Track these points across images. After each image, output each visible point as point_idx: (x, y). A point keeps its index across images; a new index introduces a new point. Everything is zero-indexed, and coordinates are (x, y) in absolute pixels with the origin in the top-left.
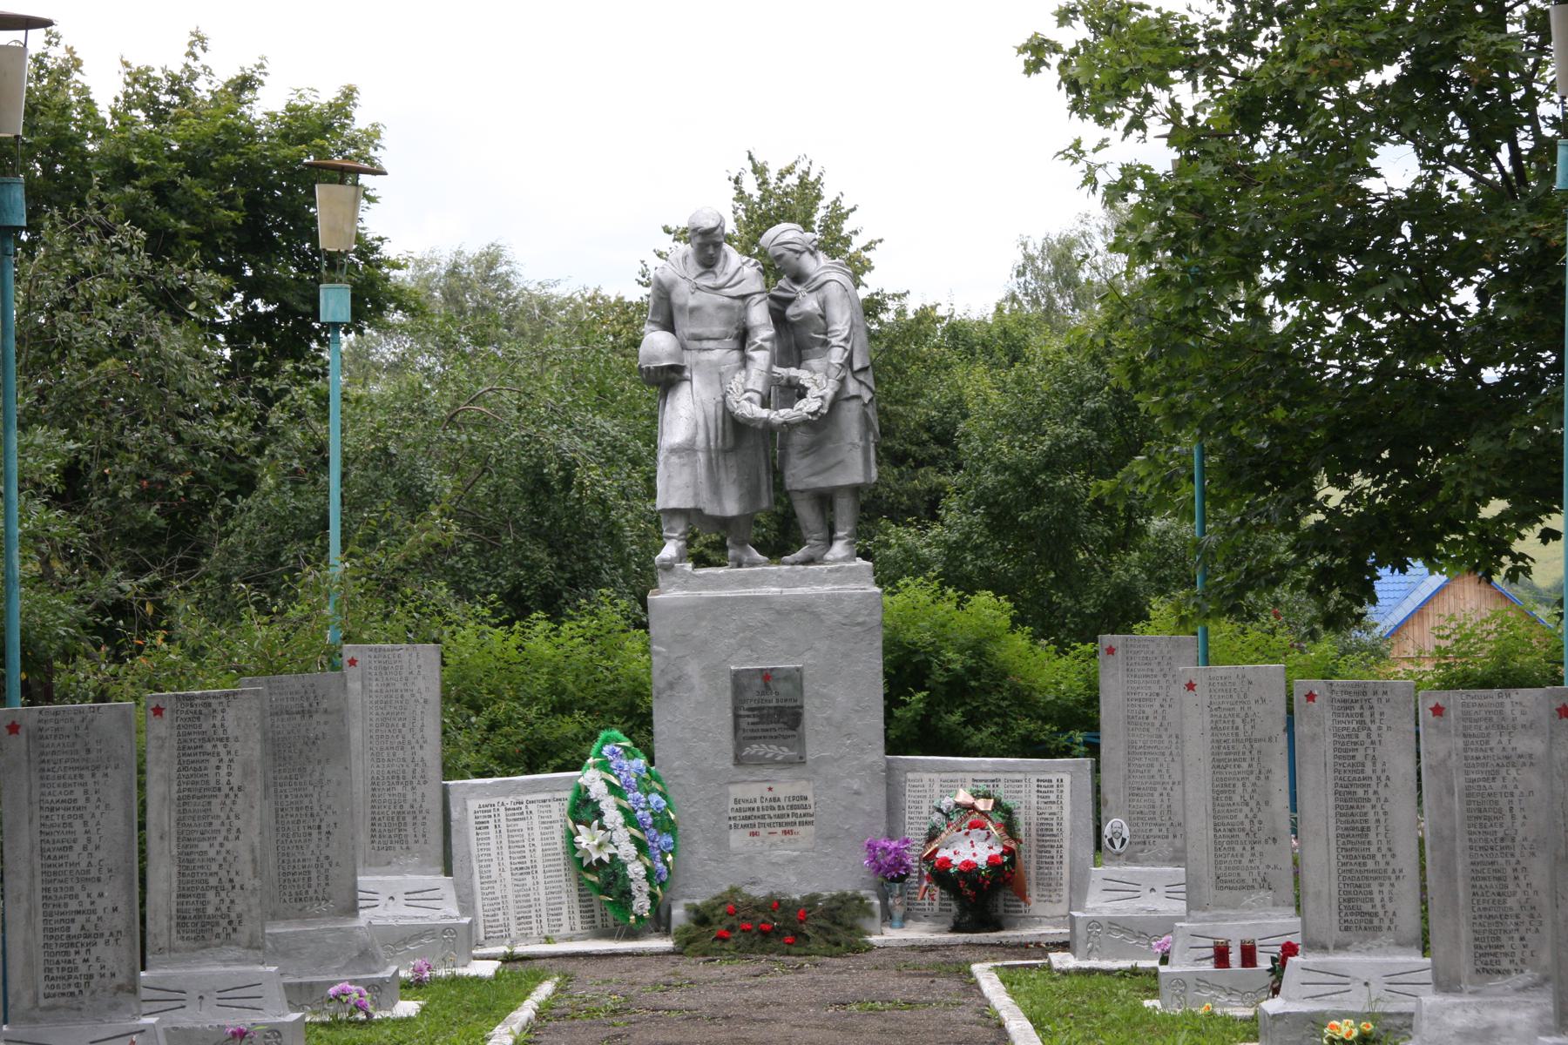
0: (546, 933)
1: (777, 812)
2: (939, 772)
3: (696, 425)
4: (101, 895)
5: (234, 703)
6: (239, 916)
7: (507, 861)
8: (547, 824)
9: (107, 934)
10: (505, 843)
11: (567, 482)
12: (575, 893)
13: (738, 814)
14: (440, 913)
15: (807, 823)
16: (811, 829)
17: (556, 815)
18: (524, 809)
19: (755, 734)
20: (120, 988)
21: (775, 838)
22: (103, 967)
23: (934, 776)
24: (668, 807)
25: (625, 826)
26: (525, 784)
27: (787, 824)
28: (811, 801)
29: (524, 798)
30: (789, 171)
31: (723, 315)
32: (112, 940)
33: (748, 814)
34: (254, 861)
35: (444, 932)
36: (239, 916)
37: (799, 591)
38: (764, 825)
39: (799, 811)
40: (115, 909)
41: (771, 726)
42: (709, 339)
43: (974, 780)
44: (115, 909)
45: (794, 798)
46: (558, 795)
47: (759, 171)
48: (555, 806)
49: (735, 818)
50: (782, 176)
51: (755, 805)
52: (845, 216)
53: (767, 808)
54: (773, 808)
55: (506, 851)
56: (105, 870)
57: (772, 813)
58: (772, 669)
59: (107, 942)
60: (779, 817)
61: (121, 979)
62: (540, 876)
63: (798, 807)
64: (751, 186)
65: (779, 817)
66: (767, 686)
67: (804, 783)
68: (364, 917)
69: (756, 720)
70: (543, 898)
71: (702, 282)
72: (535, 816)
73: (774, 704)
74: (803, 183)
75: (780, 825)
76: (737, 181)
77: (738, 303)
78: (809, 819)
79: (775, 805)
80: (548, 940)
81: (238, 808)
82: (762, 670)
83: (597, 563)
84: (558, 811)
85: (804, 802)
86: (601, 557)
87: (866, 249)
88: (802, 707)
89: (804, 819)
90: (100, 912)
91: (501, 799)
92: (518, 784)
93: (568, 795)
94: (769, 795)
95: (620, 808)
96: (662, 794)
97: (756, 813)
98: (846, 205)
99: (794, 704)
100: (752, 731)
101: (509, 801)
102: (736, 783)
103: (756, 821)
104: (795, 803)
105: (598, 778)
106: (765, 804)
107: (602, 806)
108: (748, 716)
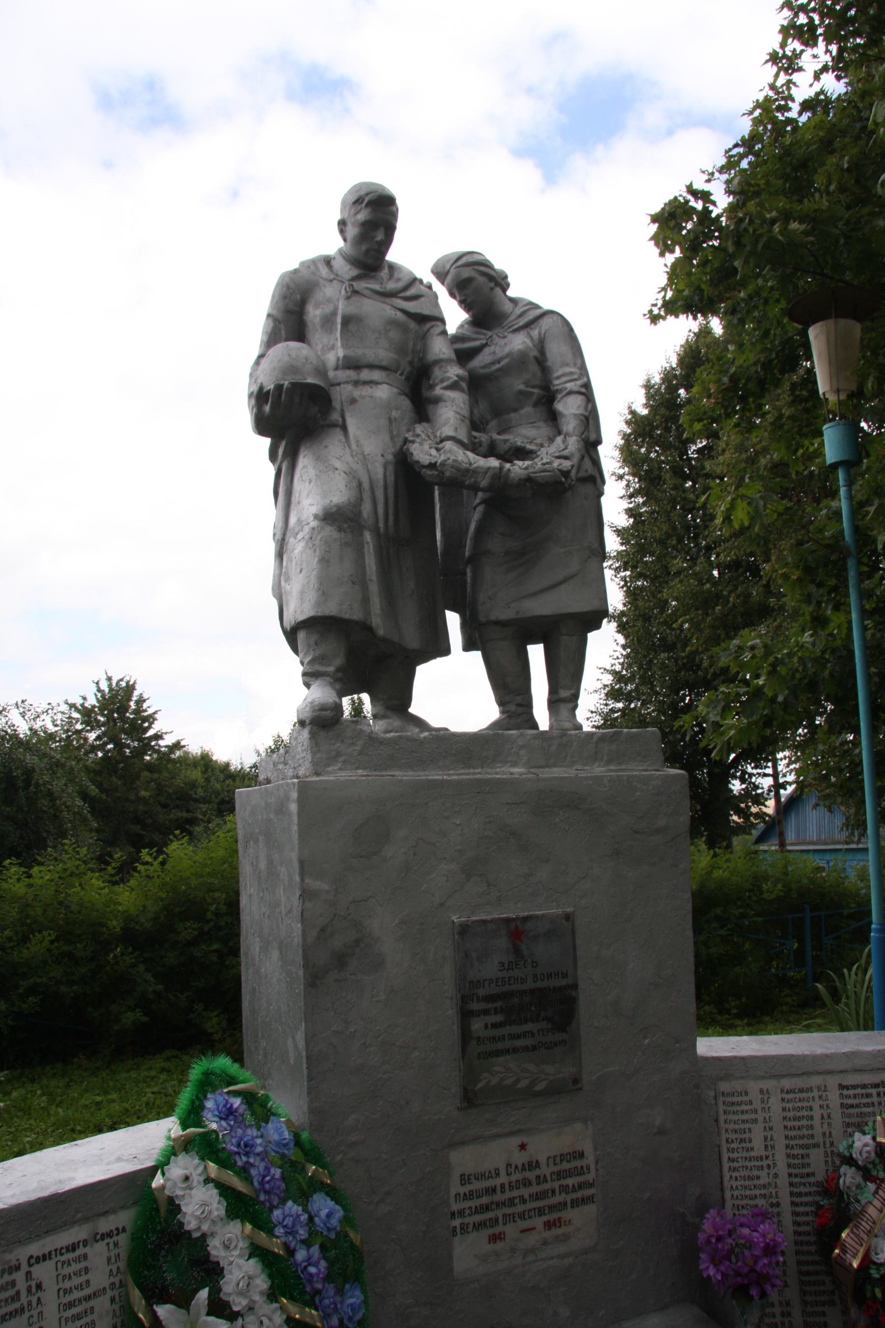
1: (535, 1189)
2: (779, 1077)
3: (360, 485)
11: (28, 782)
13: (467, 1204)
15: (585, 1201)
16: (591, 1209)
17: (100, 1278)
18: (22, 1285)
19: (500, 1046)
21: (532, 1240)
23: (770, 1084)
24: (346, 1220)
25: (272, 1296)
27: (552, 1208)
28: (590, 1159)
30: (122, 680)
31: (395, 334)
33: (484, 1200)
37: (557, 772)
38: (509, 1218)
39: (570, 1182)
41: (529, 1027)
42: (372, 367)
43: (842, 1087)
45: (563, 1157)
46: (105, 1225)
47: (109, 679)
48: (98, 1253)
49: (461, 1213)
51: (497, 1182)
52: (144, 701)
53: (518, 1185)
54: (527, 1183)
57: (525, 1192)
58: (526, 919)
60: (538, 1196)
63: (569, 1173)
64: (104, 686)
65: (538, 1196)
66: (517, 951)
67: (579, 1126)
69: (499, 1018)
71: (360, 285)
73: (529, 985)
75: (541, 1212)
76: (97, 683)
77: (412, 325)
78: (588, 1192)
79: (531, 1175)
82: (508, 921)
83: (45, 835)
85: (578, 1163)
86: (48, 832)
88: (575, 987)
89: (579, 1194)
94: (520, 1158)
95: (256, 1251)
96: (332, 1193)
97: (499, 1197)
98: (145, 696)
99: (564, 982)
100: (493, 1039)
102: (463, 1143)
103: (500, 1213)
104: (566, 1166)
105: (197, 1178)
106: (514, 1178)
107: (215, 1249)
108: (486, 1012)
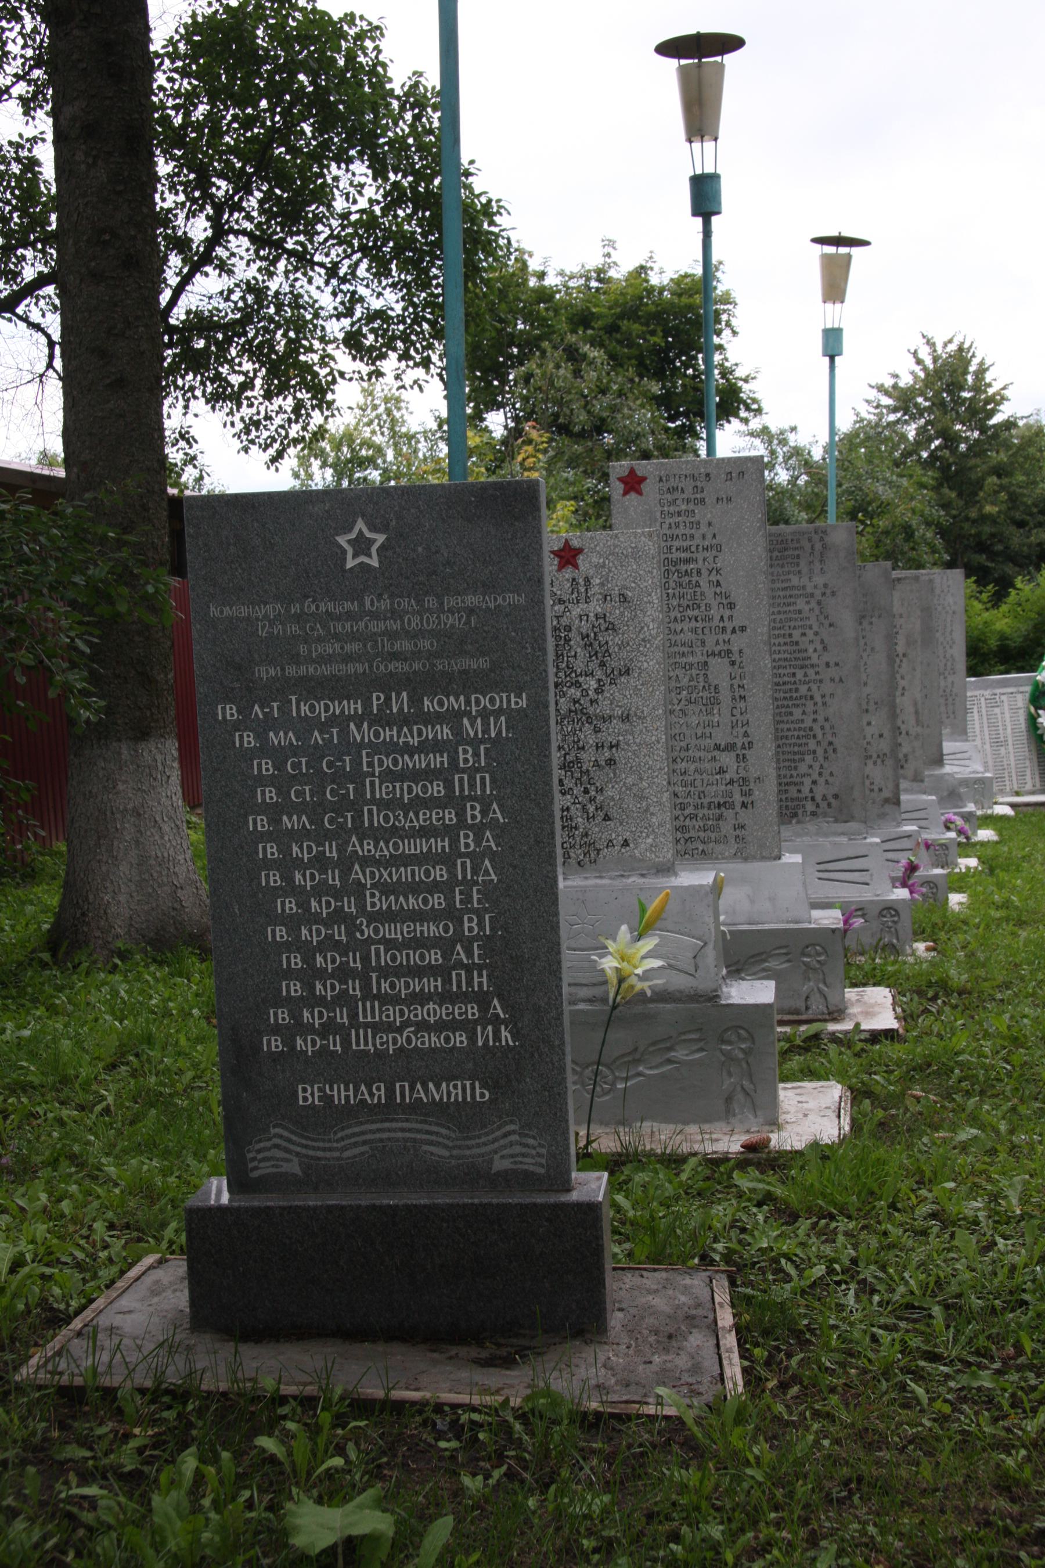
0: (1016, 788)
4: (869, 724)
5: (898, 587)
6: (906, 756)
7: (987, 737)
8: (1014, 710)
9: (875, 756)
10: (986, 725)
12: (1035, 760)
14: (969, 769)
20: (887, 801)
22: (872, 784)
26: (999, 681)
29: (998, 691)
30: (950, 341)
32: (879, 761)
34: (917, 712)
35: (975, 783)
36: (906, 756)
40: (881, 736)
44: (881, 736)
46: (1022, 689)
47: (930, 343)
48: (1019, 697)
50: (945, 345)
52: (987, 369)
55: (986, 729)
56: (872, 703)
59: (875, 763)
61: (887, 794)
62: (1010, 747)
64: (925, 354)
68: (947, 769)
70: (1013, 763)
72: (1006, 704)
74: (960, 349)
80: (1017, 794)
81: (902, 671)
84: (1022, 700)
87: (1004, 388)
90: (869, 738)
91: (982, 692)
92: (993, 681)
93: (1028, 689)
101: (987, 693)
